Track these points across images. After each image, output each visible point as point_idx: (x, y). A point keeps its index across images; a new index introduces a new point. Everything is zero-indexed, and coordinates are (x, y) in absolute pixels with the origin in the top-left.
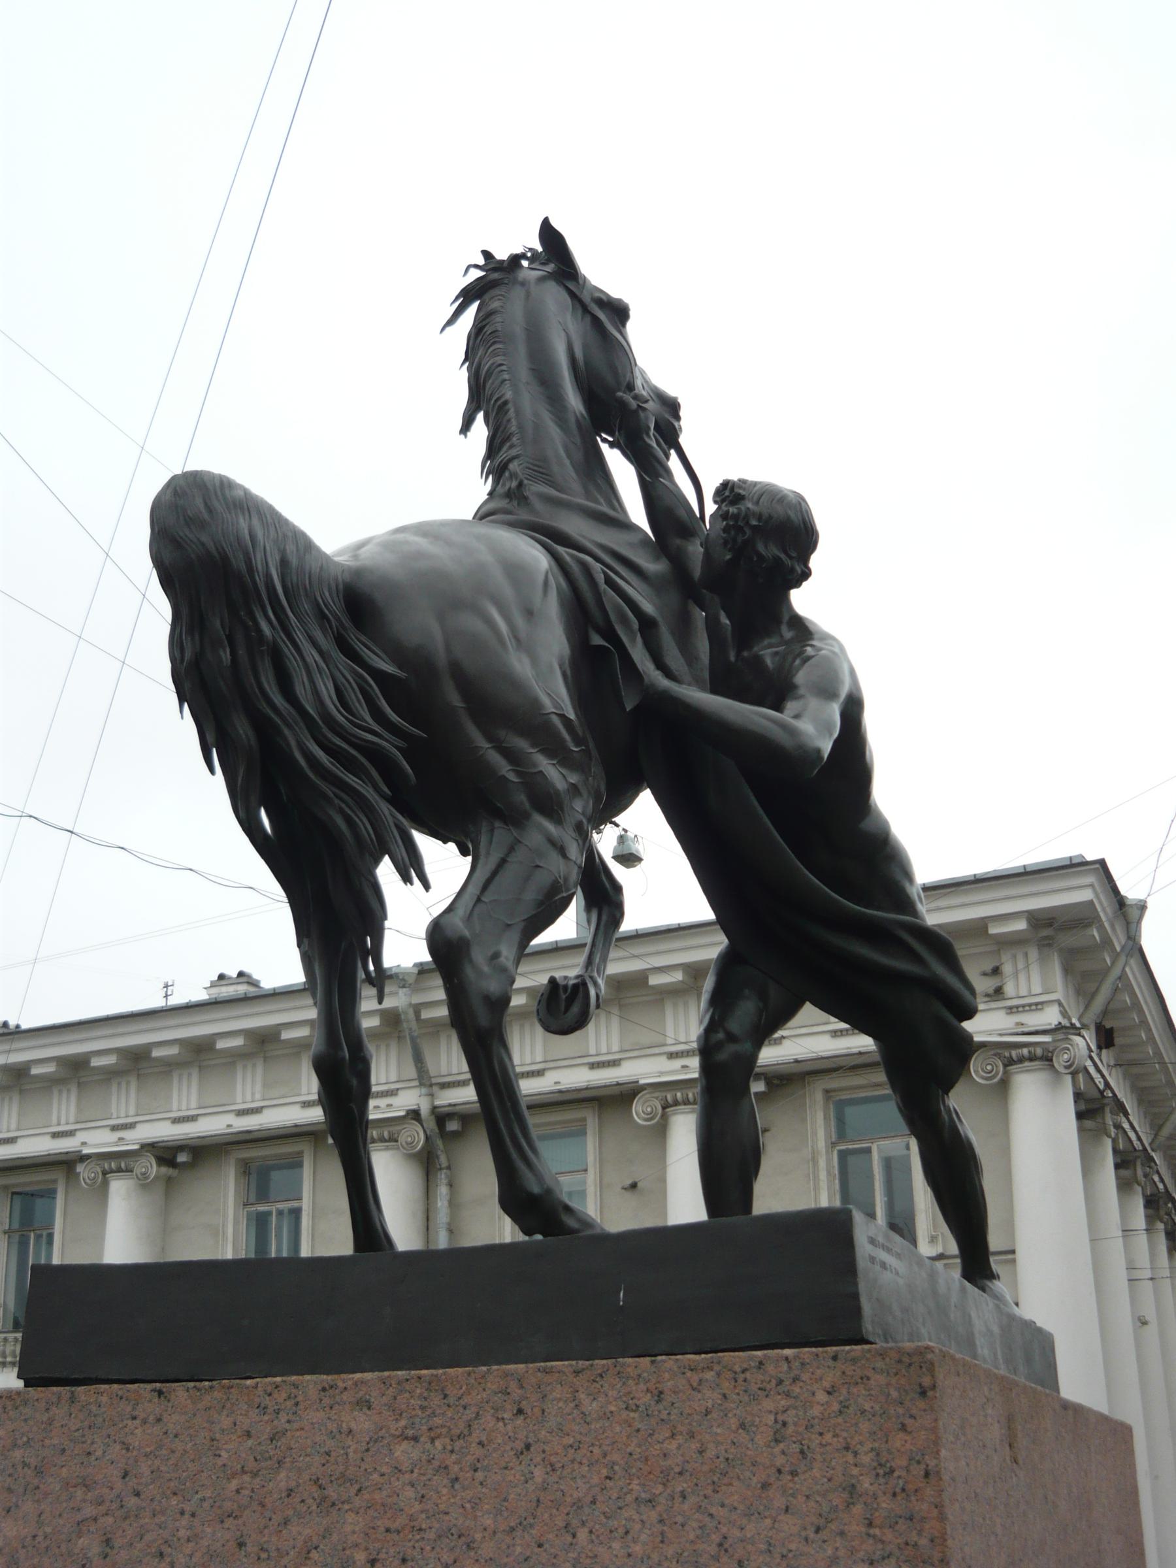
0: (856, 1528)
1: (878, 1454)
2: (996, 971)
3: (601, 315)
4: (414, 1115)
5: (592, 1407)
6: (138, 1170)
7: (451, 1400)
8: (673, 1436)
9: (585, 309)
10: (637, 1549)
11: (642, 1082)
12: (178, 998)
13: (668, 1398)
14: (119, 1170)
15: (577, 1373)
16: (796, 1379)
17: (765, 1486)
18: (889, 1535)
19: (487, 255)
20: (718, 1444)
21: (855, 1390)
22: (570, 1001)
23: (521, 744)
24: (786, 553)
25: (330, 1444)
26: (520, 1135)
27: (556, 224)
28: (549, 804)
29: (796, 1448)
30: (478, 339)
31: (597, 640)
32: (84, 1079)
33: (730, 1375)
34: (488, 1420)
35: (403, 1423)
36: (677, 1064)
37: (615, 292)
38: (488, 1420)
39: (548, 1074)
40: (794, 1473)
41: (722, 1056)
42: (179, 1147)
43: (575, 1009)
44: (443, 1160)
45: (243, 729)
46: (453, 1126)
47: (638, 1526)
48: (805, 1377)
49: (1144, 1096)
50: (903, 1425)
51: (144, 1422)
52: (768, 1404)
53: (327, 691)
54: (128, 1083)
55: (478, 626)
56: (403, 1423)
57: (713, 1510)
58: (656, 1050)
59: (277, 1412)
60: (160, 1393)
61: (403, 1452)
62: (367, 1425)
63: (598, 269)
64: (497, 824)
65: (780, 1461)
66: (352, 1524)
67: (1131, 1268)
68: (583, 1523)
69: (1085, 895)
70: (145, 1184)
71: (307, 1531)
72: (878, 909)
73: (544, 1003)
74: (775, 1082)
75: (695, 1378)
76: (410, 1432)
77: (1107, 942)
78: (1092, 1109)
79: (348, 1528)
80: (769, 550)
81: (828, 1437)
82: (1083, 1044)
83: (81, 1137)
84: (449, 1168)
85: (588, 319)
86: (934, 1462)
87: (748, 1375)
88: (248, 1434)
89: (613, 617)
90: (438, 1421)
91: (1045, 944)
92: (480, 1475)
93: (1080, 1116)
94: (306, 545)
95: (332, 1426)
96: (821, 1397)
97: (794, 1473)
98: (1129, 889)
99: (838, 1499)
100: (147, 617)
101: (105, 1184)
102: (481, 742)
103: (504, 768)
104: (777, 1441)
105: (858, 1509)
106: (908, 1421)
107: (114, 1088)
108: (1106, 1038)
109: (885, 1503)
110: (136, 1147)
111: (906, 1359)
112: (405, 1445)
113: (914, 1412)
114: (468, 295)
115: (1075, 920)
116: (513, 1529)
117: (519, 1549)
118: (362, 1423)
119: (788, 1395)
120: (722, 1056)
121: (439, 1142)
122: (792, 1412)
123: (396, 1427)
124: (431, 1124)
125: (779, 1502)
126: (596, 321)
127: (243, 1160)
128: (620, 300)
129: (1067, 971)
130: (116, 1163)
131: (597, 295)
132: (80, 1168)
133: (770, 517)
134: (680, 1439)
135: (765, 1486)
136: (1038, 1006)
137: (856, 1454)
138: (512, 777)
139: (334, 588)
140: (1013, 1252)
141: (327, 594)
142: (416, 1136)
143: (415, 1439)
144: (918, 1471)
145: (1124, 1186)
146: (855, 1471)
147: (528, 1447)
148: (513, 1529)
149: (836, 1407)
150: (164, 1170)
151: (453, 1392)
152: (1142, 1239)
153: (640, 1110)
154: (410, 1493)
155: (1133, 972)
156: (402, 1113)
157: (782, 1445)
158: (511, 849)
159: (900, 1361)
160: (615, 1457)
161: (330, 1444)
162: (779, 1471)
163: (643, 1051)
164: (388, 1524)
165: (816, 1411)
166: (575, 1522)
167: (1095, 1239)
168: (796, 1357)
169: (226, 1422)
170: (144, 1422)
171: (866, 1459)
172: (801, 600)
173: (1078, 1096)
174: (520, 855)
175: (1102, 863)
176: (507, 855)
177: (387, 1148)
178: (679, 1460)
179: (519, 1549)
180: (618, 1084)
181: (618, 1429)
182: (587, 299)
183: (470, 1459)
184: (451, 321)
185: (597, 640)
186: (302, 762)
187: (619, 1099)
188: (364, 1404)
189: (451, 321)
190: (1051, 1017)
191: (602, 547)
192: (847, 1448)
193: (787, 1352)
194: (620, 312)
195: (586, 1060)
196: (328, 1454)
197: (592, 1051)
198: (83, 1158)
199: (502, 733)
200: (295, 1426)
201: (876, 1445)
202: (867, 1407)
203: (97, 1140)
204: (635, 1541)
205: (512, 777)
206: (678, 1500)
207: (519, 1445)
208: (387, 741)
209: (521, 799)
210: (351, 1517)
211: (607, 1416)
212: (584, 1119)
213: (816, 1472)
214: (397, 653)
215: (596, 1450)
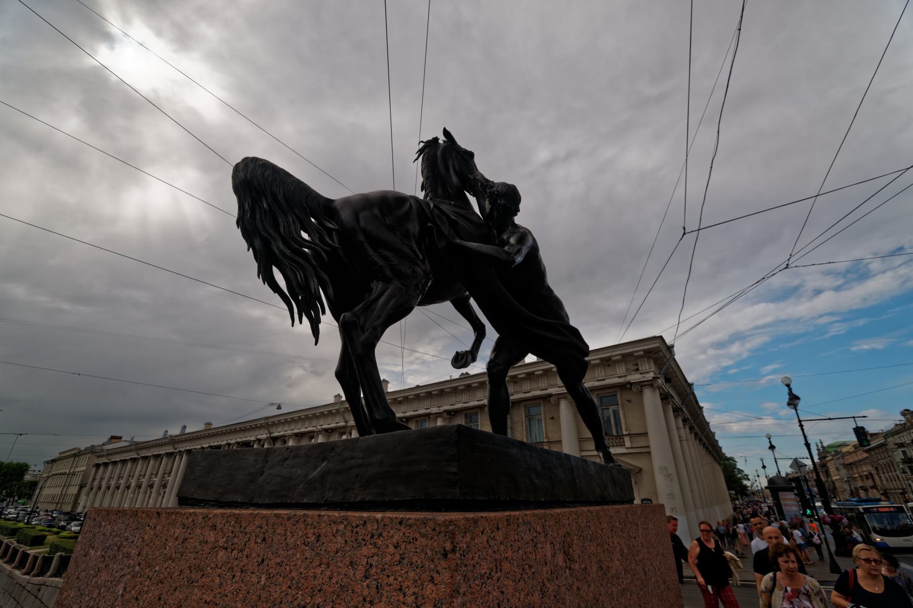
1: (416, 598)
2: (637, 364)
12: (454, 378)
13: (323, 539)
16: (380, 535)
20: (339, 574)
22: (462, 359)
23: (386, 253)
27: (447, 129)
34: (252, 544)
43: (464, 360)
45: (257, 243)
49: (680, 395)
50: (433, 578)
63: (463, 142)
67: (680, 437)
69: (657, 345)
77: (665, 356)
78: (665, 397)
81: (392, 578)
82: (661, 381)
87: (358, 529)
90: (236, 540)
91: (649, 358)
93: (662, 399)
96: (391, 549)
98: (669, 341)
102: (371, 252)
104: (366, 577)
106: (435, 575)
108: (668, 380)
113: (439, 568)
114: (421, 151)
115: (656, 351)
119: (375, 545)
122: (376, 558)
123: (221, 542)
129: (655, 363)
136: (648, 372)
143: (226, 549)
145: (676, 417)
147: (263, 560)
149: (397, 558)
152: (682, 430)
153: (552, 399)
155: (672, 363)
157: (368, 581)
159: (434, 530)
160: (294, 574)
162: (364, 600)
167: (669, 430)
172: (518, 220)
173: (661, 395)
175: (661, 337)
184: (417, 159)
186: (276, 251)
187: (546, 398)
189: (417, 159)
190: (652, 375)
199: (381, 250)
201: (416, 590)
203: (434, 410)
207: (260, 559)
209: (388, 273)
211: (296, 546)
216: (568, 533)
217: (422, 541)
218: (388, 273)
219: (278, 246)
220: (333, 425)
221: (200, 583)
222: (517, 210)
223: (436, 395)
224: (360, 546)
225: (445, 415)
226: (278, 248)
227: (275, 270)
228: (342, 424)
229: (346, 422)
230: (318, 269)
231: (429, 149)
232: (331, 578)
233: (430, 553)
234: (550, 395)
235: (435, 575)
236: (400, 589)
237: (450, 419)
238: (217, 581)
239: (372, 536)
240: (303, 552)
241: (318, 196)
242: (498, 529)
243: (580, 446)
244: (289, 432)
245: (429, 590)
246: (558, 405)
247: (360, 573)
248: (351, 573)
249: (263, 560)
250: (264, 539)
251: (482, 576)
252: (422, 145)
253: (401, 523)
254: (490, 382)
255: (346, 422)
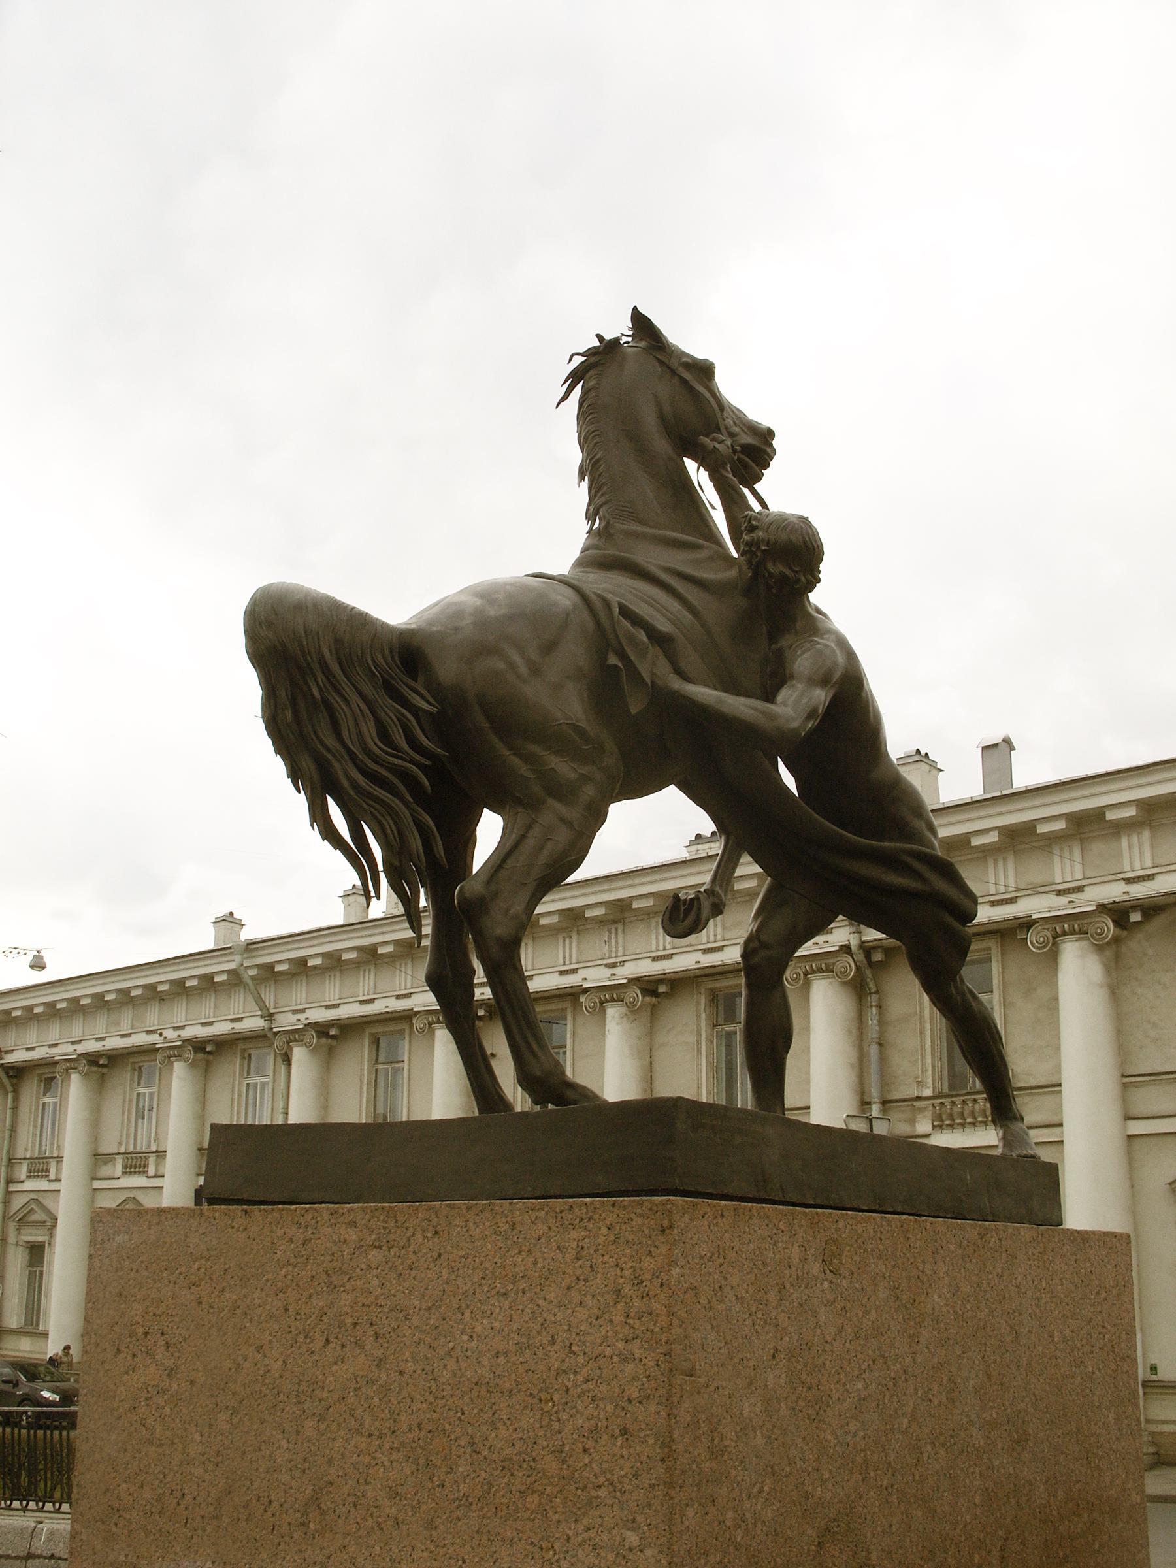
0: (618, 1319)
3: (687, 376)
4: (846, 949)
5: (476, 1232)
6: (628, 998)
7: (399, 1224)
8: (520, 1252)
9: (673, 372)
10: (497, 1324)
11: (1034, 917)
14: (613, 1000)
15: (468, 1209)
17: (569, 1288)
18: (637, 1324)
19: (599, 337)
21: (623, 1227)
24: (790, 568)
25: (335, 1248)
26: (529, 1035)
28: (559, 791)
29: (588, 1263)
30: (586, 412)
31: (613, 660)
32: (1087, 835)
33: (553, 1214)
34: (419, 1237)
35: (374, 1237)
36: (1064, 900)
37: (700, 355)
38: (419, 1237)
39: (1159, 878)
40: (586, 1281)
41: (756, 960)
42: (660, 979)
44: (872, 985)
45: (307, 763)
46: (878, 957)
47: (498, 1310)
48: (596, 1217)
51: (238, 1230)
52: (573, 1234)
53: (369, 730)
54: (1005, 860)
55: (501, 665)
56: (374, 1237)
57: (540, 1302)
58: (1047, 889)
59: (307, 1227)
60: (246, 1212)
61: (374, 1256)
62: (354, 1238)
64: (520, 810)
65: (579, 1272)
66: (346, 1300)
68: (468, 1306)
70: (633, 1011)
71: (321, 1304)
72: (891, 840)
73: (667, 914)
74: (1135, 917)
75: (533, 1215)
76: (377, 1243)
79: (342, 1303)
80: (776, 568)
81: (606, 1258)
83: (582, 973)
84: (877, 992)
85: (676, 380)
86: (666, 1278)
88: (291, 1240)
89: (624, 641)
90: (392, 1237)
92: (413, 1273)
94: (359, 621)
95: (335, 1237)
96: (604, 1230)
97: (586, 1281)
99: (609, 1298)
100: (246, 688)
101: (603, 1011)
103: (524, 769)
104: (577, 1259)
105: (621, 1306)
106: (653, 1249)
107: (1056, 851)
109: (637, 1303)
110: (625, 981)
111: (655, 1208)
112: (374, 1252)
114: (575, 377)
116: (429, 1308)
117: (432, 1321)
118: (353, 1235)
119: (585, 1228)
120: (756, 960)
121: (868, 972)
122: (587, 1240)
123: (369, 1240)
124: (860, 957)
125: (577, 1299)
126: (684, 382)
127: (712, 990)
128: (706, 360)
130: (611, 994)
131: (685, 359)
132: (582, 999)
133: (776, 542)
134: (524, 1255)
135: (569, 1288)
137: (622, 1269)
138: (531, 776)
139: (387, 651)
140: (1060, 1085)
141: (380, 656)
142: (847, 965)
143: (380, 1247)
144: (657, 1282)
146: (621, 1281)
147: (440, 1255)
148: (429, 1308)
149: (612, 1238)
150: (648, 999)
151: (401, 1219)
154: (375, 1282)
156: (836, 948)
158: (529, 827)
159: (651, 1209)
160: (488, 1265)
161: (335, 1248)
163: (1036, 890)
164: (364, 1301)
165: (601, 1240)
166: (464, 1306)
168: (592, 1203)
169: (280, 1232)
170: (238, 1230)
171: (627, 1273)
174: (536, 831)
176: (527, 832)
177: (1079, 940)
178: (523, 1268)
179: (432, 1321)
180: (1015, 918)
181: (489, 1246)
182: (675, 364)
183: (409, 1262)
185: (613, 660)
188: (353, 1224)
191: (668, 570)
192: (617, 1266)
193: (588, 1200)
194: (705, 370)
195: (1122, 876)
196: (333, 1255)
197: (1058, 879)
198: (586, 991)
200: (317, 1236)
202: (630, 1238)
203: (595, 976)
204: (496, 1319)
205: (531, 776)
206: (520, 1294)
207: (435, 1255)
208: (412, 761)
209: (537, 790)
210: (344, 1296)
211: (485, 1237)
212: (989, 949)
213: (598, 1281)
214: (437, 691)
215: (477, 1260)
216: (835, 1241)
217: (640, 1221)
218: (537, 790)
219: (343, 770)
220: (222, 1028)
221: (348, 1286)
222: (813, 580)
223: (601, 922)
224: (566, 1230)
225: (635, 995)
226: (345, 772)
227: (331, 803)
228: (254, 1023)
229: (269, 1016)
230: (415, 806)
231: (597, 367)
232: (535, 1264)
233: (647, 1231)
234: (1027, 924)
235: (653, 1249)
236: (617, 1266)
237: (654, 1010)
238: (375, 1282)
239: (582, 1219)
240: (495, 1242)
241: (384, 625)
242: (722, 1216)
243: (1125, 1101)
244: (66, 1050)
245: (647, 1263)
246: (1053, 957)
247: (570, 1255)
248: (559, 1256)
249: (440, 1255)
250: (436, 1232)
251: (702, 1257)
252: (578, 360)
253: (613, 1205)
254: (749, 985)
255: (269, 1016)
